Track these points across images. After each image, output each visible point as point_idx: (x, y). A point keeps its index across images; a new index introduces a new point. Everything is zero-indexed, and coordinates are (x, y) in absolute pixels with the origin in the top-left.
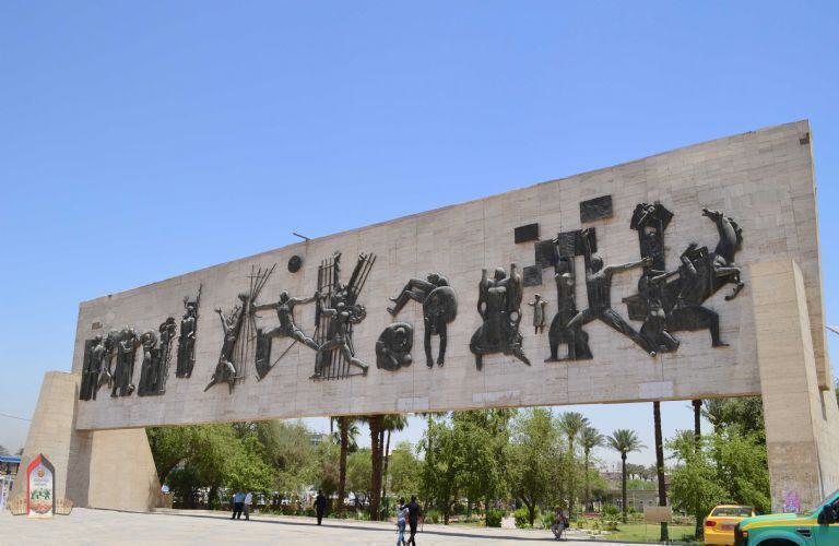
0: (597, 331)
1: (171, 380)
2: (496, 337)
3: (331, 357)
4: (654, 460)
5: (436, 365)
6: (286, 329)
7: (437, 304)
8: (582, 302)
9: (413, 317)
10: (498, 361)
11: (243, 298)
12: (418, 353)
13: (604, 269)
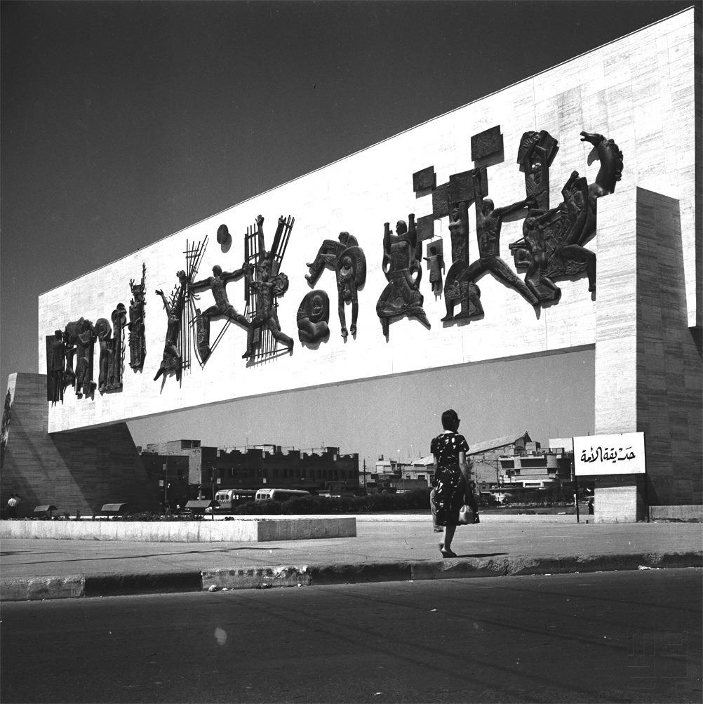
0: (488, 285)
1: (128, 373)
3: (261, 327)
4: (580, 516)
5: (350, 336)
6: (222, 310)
8: (474, 255)
9: (328, 282)
10: (404, 327)
11: (181, 275)
12: (334, 324)
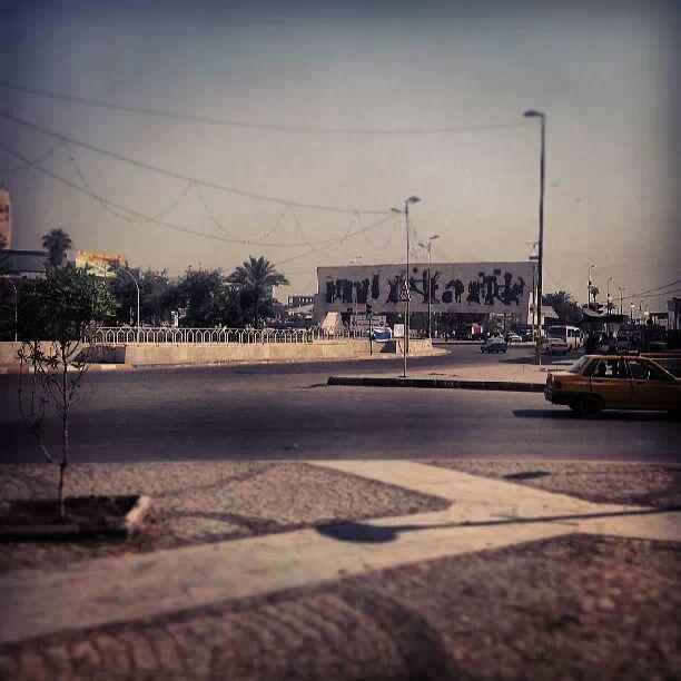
0: (495, 299)
2: (473, 298)
7: (459, 288)
12: (453, 299)
13: (466, 288)
